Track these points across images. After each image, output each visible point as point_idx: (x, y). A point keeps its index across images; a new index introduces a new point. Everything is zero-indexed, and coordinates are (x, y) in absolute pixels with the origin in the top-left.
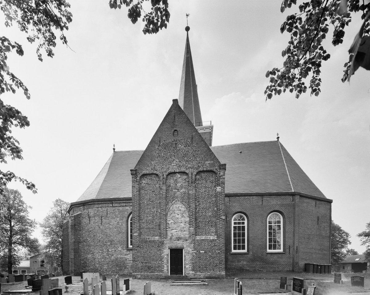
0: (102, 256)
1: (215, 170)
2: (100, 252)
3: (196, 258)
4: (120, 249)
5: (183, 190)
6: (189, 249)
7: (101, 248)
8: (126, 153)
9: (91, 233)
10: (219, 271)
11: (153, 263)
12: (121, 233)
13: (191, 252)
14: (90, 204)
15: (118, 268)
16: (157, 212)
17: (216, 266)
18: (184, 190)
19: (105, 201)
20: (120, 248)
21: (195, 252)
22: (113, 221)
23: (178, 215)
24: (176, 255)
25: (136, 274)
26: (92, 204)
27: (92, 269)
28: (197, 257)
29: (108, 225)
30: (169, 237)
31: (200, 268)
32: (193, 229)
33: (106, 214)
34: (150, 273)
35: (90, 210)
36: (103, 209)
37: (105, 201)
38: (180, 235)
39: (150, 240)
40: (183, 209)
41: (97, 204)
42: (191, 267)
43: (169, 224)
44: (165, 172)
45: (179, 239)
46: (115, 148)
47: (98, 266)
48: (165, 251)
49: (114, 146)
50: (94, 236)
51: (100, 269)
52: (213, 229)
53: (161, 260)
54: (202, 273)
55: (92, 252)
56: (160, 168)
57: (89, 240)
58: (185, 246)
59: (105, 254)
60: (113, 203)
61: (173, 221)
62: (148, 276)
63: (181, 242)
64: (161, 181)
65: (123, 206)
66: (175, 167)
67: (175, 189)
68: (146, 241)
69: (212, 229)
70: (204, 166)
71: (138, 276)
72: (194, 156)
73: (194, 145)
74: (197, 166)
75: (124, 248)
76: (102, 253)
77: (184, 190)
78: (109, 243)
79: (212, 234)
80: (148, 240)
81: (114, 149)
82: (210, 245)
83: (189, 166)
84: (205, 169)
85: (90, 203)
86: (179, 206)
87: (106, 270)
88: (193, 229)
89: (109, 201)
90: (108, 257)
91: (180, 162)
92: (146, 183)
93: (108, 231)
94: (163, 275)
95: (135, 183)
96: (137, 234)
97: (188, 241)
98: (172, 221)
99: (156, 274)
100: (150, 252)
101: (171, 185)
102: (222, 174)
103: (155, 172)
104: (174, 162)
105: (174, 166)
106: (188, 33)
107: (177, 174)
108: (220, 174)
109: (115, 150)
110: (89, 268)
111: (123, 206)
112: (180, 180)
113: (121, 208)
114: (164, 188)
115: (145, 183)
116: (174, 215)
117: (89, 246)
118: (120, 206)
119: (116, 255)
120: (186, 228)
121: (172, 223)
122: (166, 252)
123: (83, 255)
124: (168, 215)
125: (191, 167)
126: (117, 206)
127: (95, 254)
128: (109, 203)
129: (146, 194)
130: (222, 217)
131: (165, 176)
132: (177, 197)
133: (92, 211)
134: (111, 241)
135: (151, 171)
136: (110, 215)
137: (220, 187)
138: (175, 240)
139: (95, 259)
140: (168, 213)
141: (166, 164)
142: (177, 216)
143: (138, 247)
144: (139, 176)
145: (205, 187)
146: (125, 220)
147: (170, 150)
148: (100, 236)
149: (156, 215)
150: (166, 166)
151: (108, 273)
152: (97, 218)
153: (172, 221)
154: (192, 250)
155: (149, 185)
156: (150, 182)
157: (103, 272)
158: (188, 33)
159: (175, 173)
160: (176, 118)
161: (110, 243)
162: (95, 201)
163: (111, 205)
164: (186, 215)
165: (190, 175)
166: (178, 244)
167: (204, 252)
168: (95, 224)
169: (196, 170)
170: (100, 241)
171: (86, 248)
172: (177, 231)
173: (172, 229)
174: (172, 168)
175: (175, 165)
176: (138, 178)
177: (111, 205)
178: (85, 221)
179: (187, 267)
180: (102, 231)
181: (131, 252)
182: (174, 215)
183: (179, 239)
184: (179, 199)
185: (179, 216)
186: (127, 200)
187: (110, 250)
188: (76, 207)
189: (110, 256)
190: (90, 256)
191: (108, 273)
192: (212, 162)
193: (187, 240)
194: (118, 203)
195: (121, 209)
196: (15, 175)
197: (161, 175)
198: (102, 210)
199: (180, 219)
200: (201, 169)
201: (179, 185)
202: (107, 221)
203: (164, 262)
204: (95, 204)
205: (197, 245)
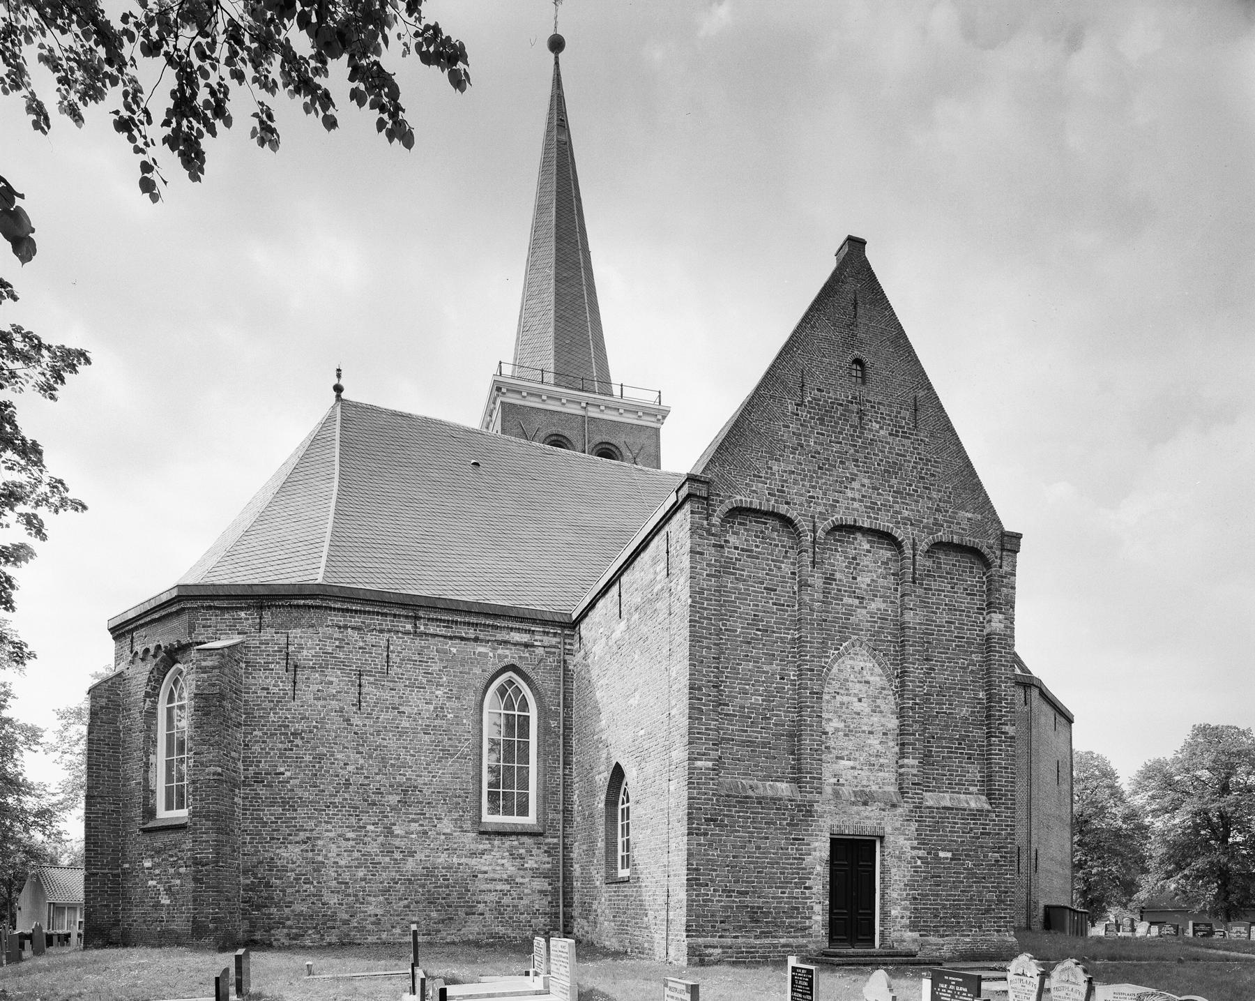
0: (356, 854)
1: (985, 550)
2: (350, 835)
3: (926, 878)
4: (446, 826)
5: (877, 605)
6: (901, 841)
7: (353, 820)
8: (399, 420)
9: (298, 742)
10: (998, 931)
11: (773, 897)
12: (452, 755)
13: (910, 853)
14: (298, 606)
15: (434, 914)
16: (782, 678)
17: (987, 911)
18: (883, 606)
19: (383, 603)
20: (445, 821)
21: (921, 853)
22: (415, 696)
23: (860, 700)
24: (853, 859)
25: (700, 940)
26: (310, 607)
27: (301, 914)
28: (930, 874)
29: (390, 715)
30: (828, 790)
31: (936, 916)
32: (916, 762)
33: (380, 662)
34: (756, 937)
35: (295, 633)
36: (370, 638)
37: (383, 603)
38: (865, 783)
39: (760, 792)
40: (878, 679)
41: (339, 610)
42: (908, 913)
43: (826, 733)
44: (823, 516)
45: (865, 799)
46: (342, 383)
47: (333, 900)
48: (817, 844)
49: (339, 376)
50: (320, 757)
51: (346, 917)
52: (974, 772)
53: (801, 884)
54: (942, 936)
55: (302, 835)
56: (801, 495)
57: (288, 774)
58: (888, 829)
59: (373, 848)
60: (417, 618)
61: (842, 725)
62: (751, 950)
63: (877, 812)
64: (806, 551)
65: (462, 639)
66: (856, 505)
67: (852, 594)
68: (746, 797)
69: (971, 768)
70: (955, 528)
71: (710, 951)
72: (923, 478)
73: (922, 436)
74: (931, 521)
75: (468, 825)
76: (358, 840)
77: (883, 606)
78: (394, 799)
79: (971, 788)
80: (750, 793)
81: (338, 389)
82: (971, 829)
83: (906, 513)
84: (956, 540)
85: (302, 602)
86: (862, 664)
87: (377, 923)
88: (916, 762)
89: (403, 606)
90: (387, 859)
91: (874, 488)
92: (742, 550)
93: (391, 742)
94: (811, 947)
95: (701, 536)
96: (710, 764)
97: (900, 810)
98: (836, 724)
99: (783, 941)
100: (758, 848)
101: (838, 576)
102: (1006, 568)
103: (783, 509)
104: (856, 485)
105: (854, 499)
106: (557, 58)
107: (859, 536)
108: (1001, 567)
109: (343, 395)
110: (287, 910)
111: (462, 639)
112: (866, 561)
113: (454, 648)
114: (817, 581)
115: (736, 548)
116: (845, 699)
117: (289, 804)
118: (451, 638)
119: (427, 852)
120: (889, 759)
121: (837, 730)
122: (820, 849)
123: (249, 848)
124: (826, 697)
125: (910, 520)
126: (434, 636)
127: (320, 843)
128: (399, 616)
129: (743, 596)
130: (1006, 728)
131: (820, 533)
132: (857, 629)
133: (308, 640)
134: (406, 791)
135: (768, 500)
136: (400, 671)
137: (1001, 616)
138: (853, 803)
139: (318, 867)
140: (826, 690)
141: (825, 484)
142: (857, 706)
143: (712, 820)
144: (721, 510)
145: (952, 609)
146: (471, 699)
147: (840, 433)
148: (347, 761)
149: (780, 690)
150: (825, 494)
151: (384, 936)
152: (334, 676)
153: (836, 724)
154: (913, 848)
155: (753, 557)
156: (757, 546)
157: (361, 929)
158: (557, 58)
159: (853, 529)
160: (860, 311)
161: (398, 798)
162: (335, 598)
163: (409, 627)
164: (889, 704)
165: (908, 552)
166: (863, 820)
167: (949, 855)
168: (322, 702)
169: (929, 534)
170: (347, 784)
171: (267, 814)
172: (857, 764)
173: (837, 758)
174: (847, 508)
175: (857, 496)
176: (715, 520)
177: (409, 627)
178: (267, 681)
179: (893, 912)
180: (361, 737)
181: (496, 842)
182: (845, 699)
183: (865, 799)
184: (865, 639)
185: (864, 707)
186: (487, 615)
187: (398, 830)
188: (210, 608)
189: (398, 856)
190: (291, 853)
191: (384, 936)
192: (979, 517)
193: (894, 806)
194: (441, 620)
195: (454, 650)
196: (45, 341)
197: (805, 526)
198: (361, 644)
199: (866, 720)
200: (942, 535)
201: (864, 580)
202: (386, 695)
203: (814, 890)
204: (330, 608)
205: (930, 826)
